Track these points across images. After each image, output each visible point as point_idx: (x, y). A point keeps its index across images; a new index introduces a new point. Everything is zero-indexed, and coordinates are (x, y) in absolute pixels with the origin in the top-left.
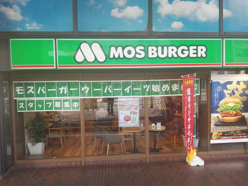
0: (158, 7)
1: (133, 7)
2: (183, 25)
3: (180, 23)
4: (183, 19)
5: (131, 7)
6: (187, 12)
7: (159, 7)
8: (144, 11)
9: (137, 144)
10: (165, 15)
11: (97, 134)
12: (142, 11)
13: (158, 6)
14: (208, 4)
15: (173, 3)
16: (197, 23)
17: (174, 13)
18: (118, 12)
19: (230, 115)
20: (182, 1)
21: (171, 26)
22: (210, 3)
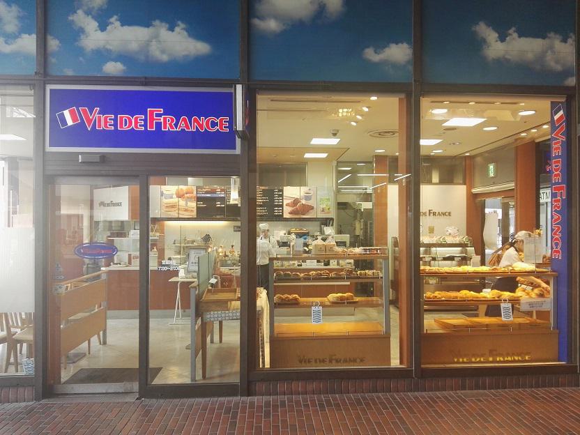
0: (80, 36)
1: (400, 45)
2: (125, 68)
3: (119, 63)
4: (123, 57)
5: (29, 35)
6: (134, 46)
7: (82, 37)
8: (60, 42)
9: (449, 240)
10: (92, 49)
11: (263, 337)
12: (405, 45)
13: (81, 34)
14: (173, 31)
15: (107, 30)
16: (151, 63)
17: (108, 47)
18: (4, 42)
19: (299, 279)
20: (124, 27)
21: (102, 69)
22: (177, 29)
